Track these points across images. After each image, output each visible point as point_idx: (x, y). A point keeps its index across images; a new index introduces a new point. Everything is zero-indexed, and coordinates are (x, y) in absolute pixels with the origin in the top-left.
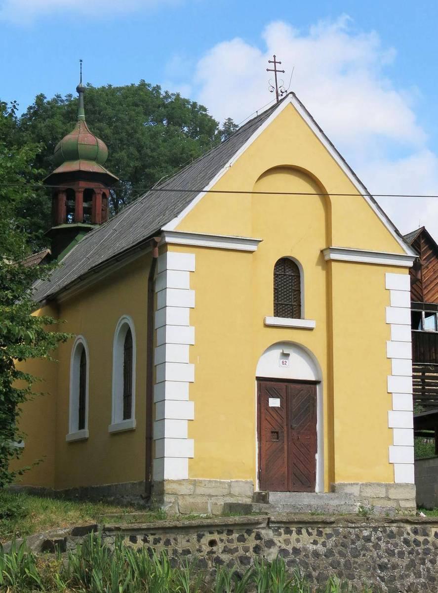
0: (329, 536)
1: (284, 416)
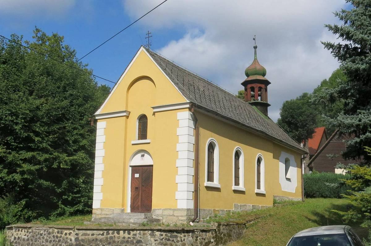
0: (30, 233)
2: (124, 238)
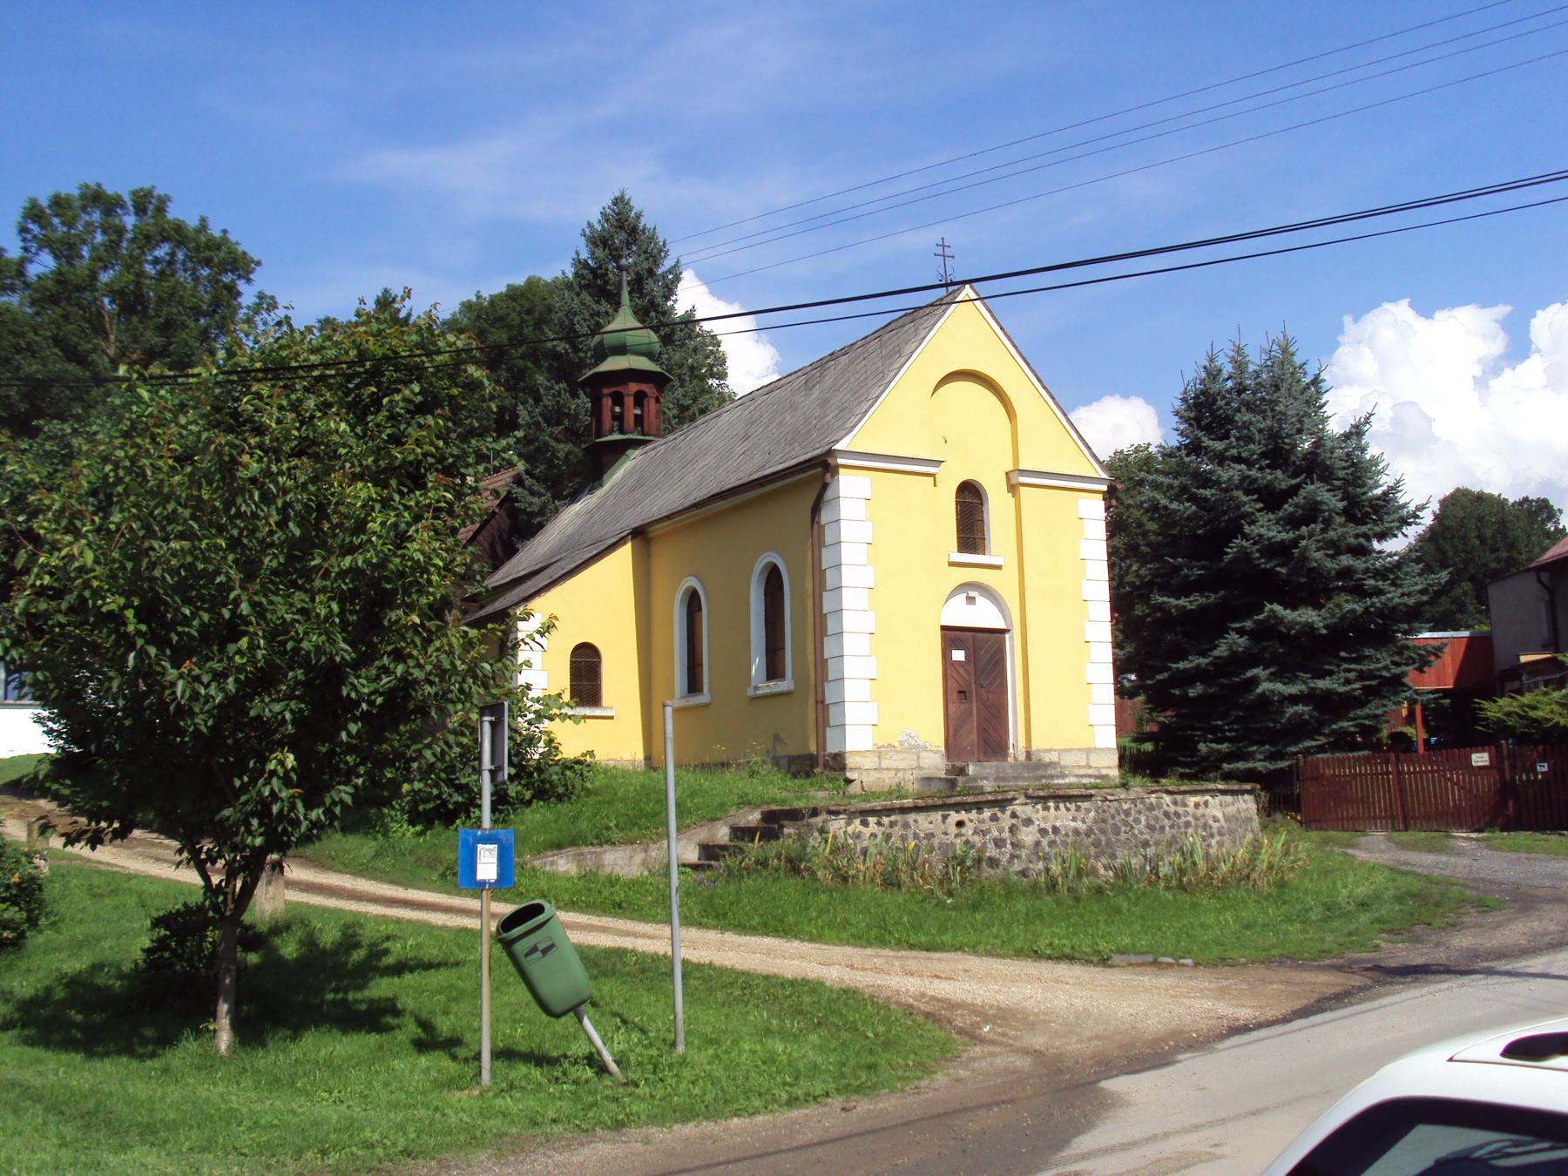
1: (972, 672)
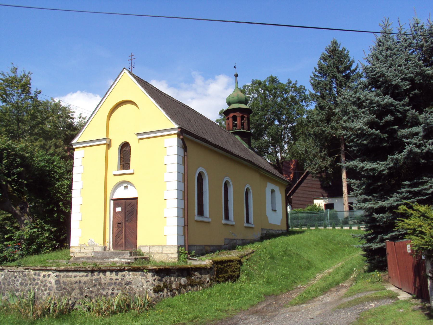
2: (111, 279)
